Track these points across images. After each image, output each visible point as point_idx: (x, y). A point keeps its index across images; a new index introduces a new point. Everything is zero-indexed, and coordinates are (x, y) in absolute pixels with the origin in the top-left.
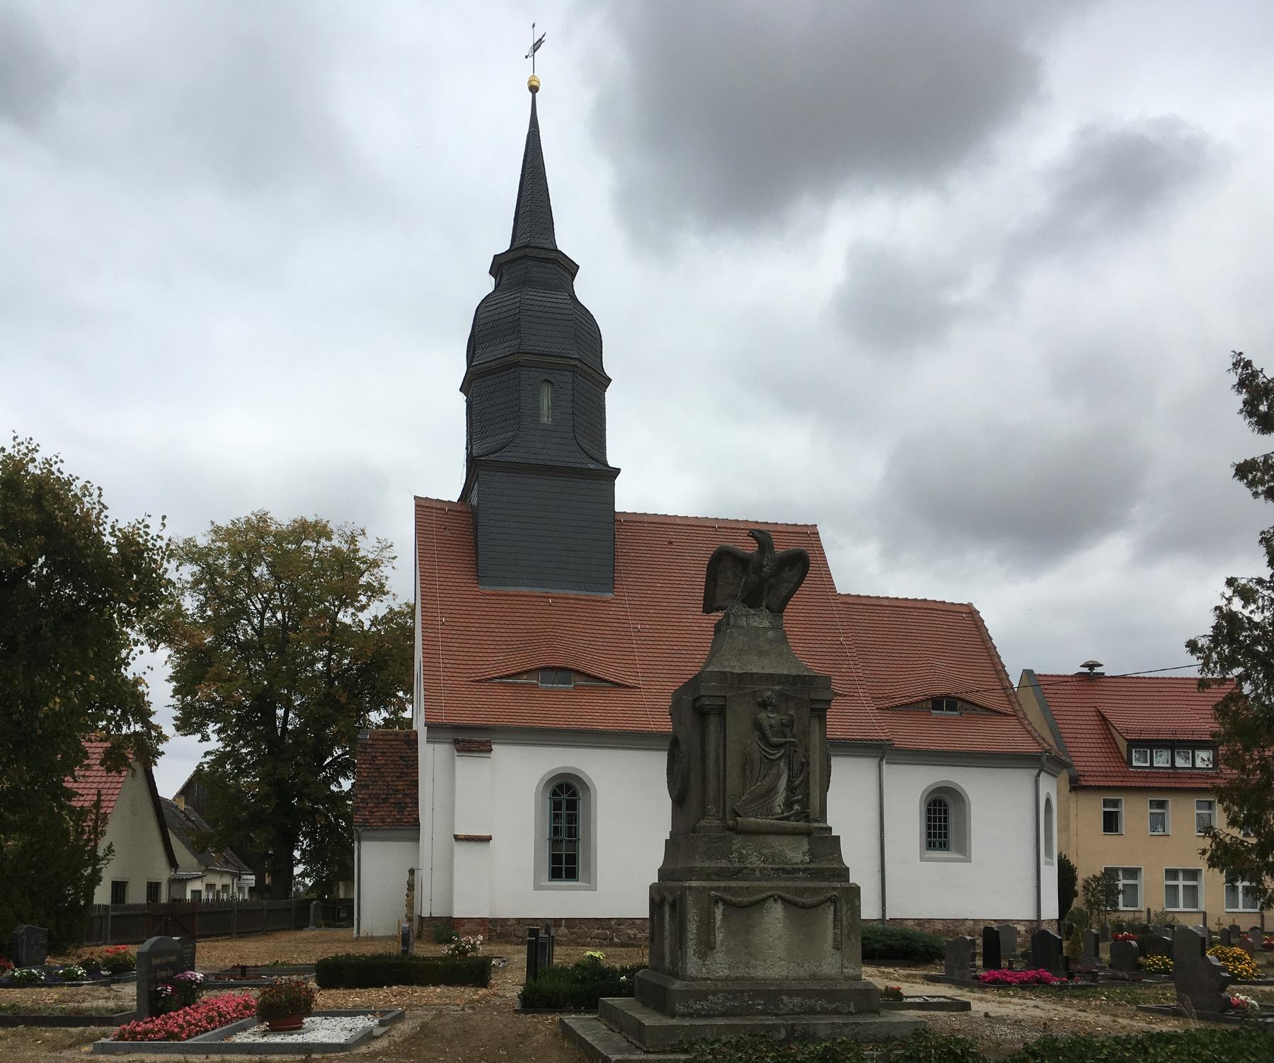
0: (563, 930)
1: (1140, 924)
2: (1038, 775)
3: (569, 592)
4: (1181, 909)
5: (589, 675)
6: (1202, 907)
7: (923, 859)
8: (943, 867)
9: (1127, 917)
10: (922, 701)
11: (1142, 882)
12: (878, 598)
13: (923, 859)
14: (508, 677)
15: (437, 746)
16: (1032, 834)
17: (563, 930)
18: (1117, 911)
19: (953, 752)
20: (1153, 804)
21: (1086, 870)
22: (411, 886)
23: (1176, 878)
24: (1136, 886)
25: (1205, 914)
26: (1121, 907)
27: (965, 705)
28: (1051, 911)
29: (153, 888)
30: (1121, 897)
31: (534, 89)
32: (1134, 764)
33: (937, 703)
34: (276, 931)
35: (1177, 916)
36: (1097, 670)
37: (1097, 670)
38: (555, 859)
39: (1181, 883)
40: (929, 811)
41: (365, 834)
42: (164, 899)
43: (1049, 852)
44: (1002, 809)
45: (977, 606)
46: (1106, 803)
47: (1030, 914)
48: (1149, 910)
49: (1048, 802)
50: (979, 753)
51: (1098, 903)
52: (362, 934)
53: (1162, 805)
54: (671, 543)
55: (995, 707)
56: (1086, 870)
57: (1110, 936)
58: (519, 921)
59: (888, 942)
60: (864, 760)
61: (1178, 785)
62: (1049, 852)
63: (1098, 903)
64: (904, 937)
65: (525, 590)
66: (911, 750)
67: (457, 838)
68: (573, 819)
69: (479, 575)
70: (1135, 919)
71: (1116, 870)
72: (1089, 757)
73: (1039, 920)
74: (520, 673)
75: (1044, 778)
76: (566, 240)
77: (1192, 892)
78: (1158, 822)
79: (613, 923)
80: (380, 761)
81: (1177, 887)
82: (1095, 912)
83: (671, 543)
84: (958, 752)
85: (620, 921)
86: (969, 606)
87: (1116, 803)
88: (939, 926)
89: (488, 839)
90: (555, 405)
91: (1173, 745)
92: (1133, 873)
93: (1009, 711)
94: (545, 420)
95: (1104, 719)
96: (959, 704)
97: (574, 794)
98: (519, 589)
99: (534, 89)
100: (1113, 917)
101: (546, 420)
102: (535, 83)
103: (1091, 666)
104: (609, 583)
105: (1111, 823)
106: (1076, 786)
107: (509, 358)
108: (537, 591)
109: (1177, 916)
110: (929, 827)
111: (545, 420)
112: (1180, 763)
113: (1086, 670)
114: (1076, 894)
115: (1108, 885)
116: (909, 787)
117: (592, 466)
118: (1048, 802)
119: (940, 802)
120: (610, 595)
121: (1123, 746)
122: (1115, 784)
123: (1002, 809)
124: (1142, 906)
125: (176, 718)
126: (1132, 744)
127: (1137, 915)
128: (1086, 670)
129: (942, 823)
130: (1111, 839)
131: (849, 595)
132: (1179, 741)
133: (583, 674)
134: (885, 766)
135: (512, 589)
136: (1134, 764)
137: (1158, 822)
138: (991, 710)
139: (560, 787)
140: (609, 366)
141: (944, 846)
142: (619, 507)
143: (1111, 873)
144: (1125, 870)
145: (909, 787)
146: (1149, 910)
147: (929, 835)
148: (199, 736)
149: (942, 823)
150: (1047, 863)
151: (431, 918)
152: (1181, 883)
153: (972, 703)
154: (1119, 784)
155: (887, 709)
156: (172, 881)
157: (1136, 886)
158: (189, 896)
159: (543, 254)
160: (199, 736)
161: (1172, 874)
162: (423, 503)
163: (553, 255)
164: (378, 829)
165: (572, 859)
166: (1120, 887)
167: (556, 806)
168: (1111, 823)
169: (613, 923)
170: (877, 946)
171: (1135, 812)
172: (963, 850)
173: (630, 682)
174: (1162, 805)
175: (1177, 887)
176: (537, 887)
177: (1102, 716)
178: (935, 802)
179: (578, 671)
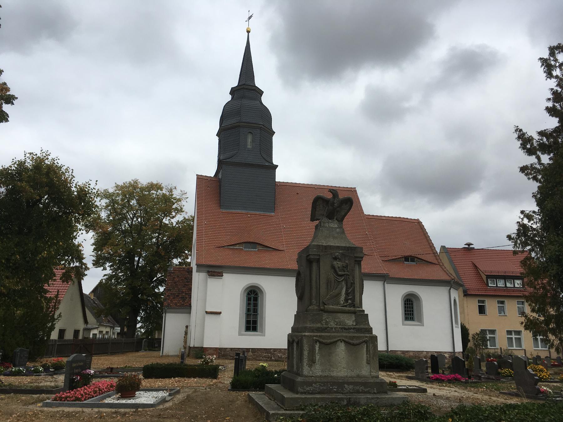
0: (250, 353)
1: (498, 354)
2: (450, 289)
4: (515, 348)
5: (264, 245)
6: (524, 347)
8: (411, 328)
9: (492, 351)
17: (250, 353)
19: (414, 279)
21: (473, 330)
22: (186, 333)
23: (511, 334)
24: (494, 338)
25: (525, 350)
26: (489, 347)
28: (459, 348)
29: (76, 332)
30: (488, 342)
31: (248, 32)
33: (407, 259)
35: (513, 351)
36: (471, 246)
37: (471, 246)
38: (248, 322)
40: (405, 304)
41: (168, 310)
42: (80, 337)
45: (421, 220)
47: (450, 350)
48: (501, 348)
49: (455, 300)
51: (479, 345)
52: (164, 354)
55: (430, 261)
56: (473, 330)
58: (231, 349)
59: (390, 361)
63: (479, 345)
67: (207, 312)
71: (485, 330)
72: (471, 282)
73: (454, 352)
74: (235, 244)
75: (452, 290)
76: (259, 83)
77: (519, 340)
78: (501, 310)
82: (478, 349)
84: (416, 279)
85: (275, 350)
87: (483, 302)
88: (411, 354)
90: (253, 141)
91: (505, 278)
92: (493, 332)
93: (436, 262)
94: (249, 147)
96: (416, 259)
97: (257, 294)
99: (248, 32)
100: (486, 351)
101: (249, 146)
103: (469, 245)
105: (482, 310)
106: (466, 294)
108: (244, 212)
109: (513, 351)
110: (405, 311)
111: (249, 147)
113: (467, 246)
115: (483, 337)
116: (396, 293)
118: (455, 300)
120: (273, 214)
121: (484, 277)
123: (436, 303)
124: (498, 346)
126: (488, 277)
127: (496, 350)
128: (467, 246)
129: (411, 309)
130: (482, 317)
134: (386, 285)
137: (501, 310)
139: (251, 291)
141: (412, 319)
143: (483, 332)
144: (489, 330)
146: (501, 348)
147: (406, 314)
148: (102, 268)
149: (411, 309)
150: (456, 327)
151: (194, 347)
152: (514, 336)
157: (494, 338)
158: (91, 336)
159: (250, 87)
160: (102, 268)
161: (509, 332)
163: (254, 88)
165: (255, 322)
166: (488, 338)
167: (249, 299)
168: (482, 310)
169: (272, 350)
170: (385, 363)
171: (491, 305)
172: (420, 321)
173: (281, 248)
174: (502, 302)
175: (512, 338)
176: (240, 334)
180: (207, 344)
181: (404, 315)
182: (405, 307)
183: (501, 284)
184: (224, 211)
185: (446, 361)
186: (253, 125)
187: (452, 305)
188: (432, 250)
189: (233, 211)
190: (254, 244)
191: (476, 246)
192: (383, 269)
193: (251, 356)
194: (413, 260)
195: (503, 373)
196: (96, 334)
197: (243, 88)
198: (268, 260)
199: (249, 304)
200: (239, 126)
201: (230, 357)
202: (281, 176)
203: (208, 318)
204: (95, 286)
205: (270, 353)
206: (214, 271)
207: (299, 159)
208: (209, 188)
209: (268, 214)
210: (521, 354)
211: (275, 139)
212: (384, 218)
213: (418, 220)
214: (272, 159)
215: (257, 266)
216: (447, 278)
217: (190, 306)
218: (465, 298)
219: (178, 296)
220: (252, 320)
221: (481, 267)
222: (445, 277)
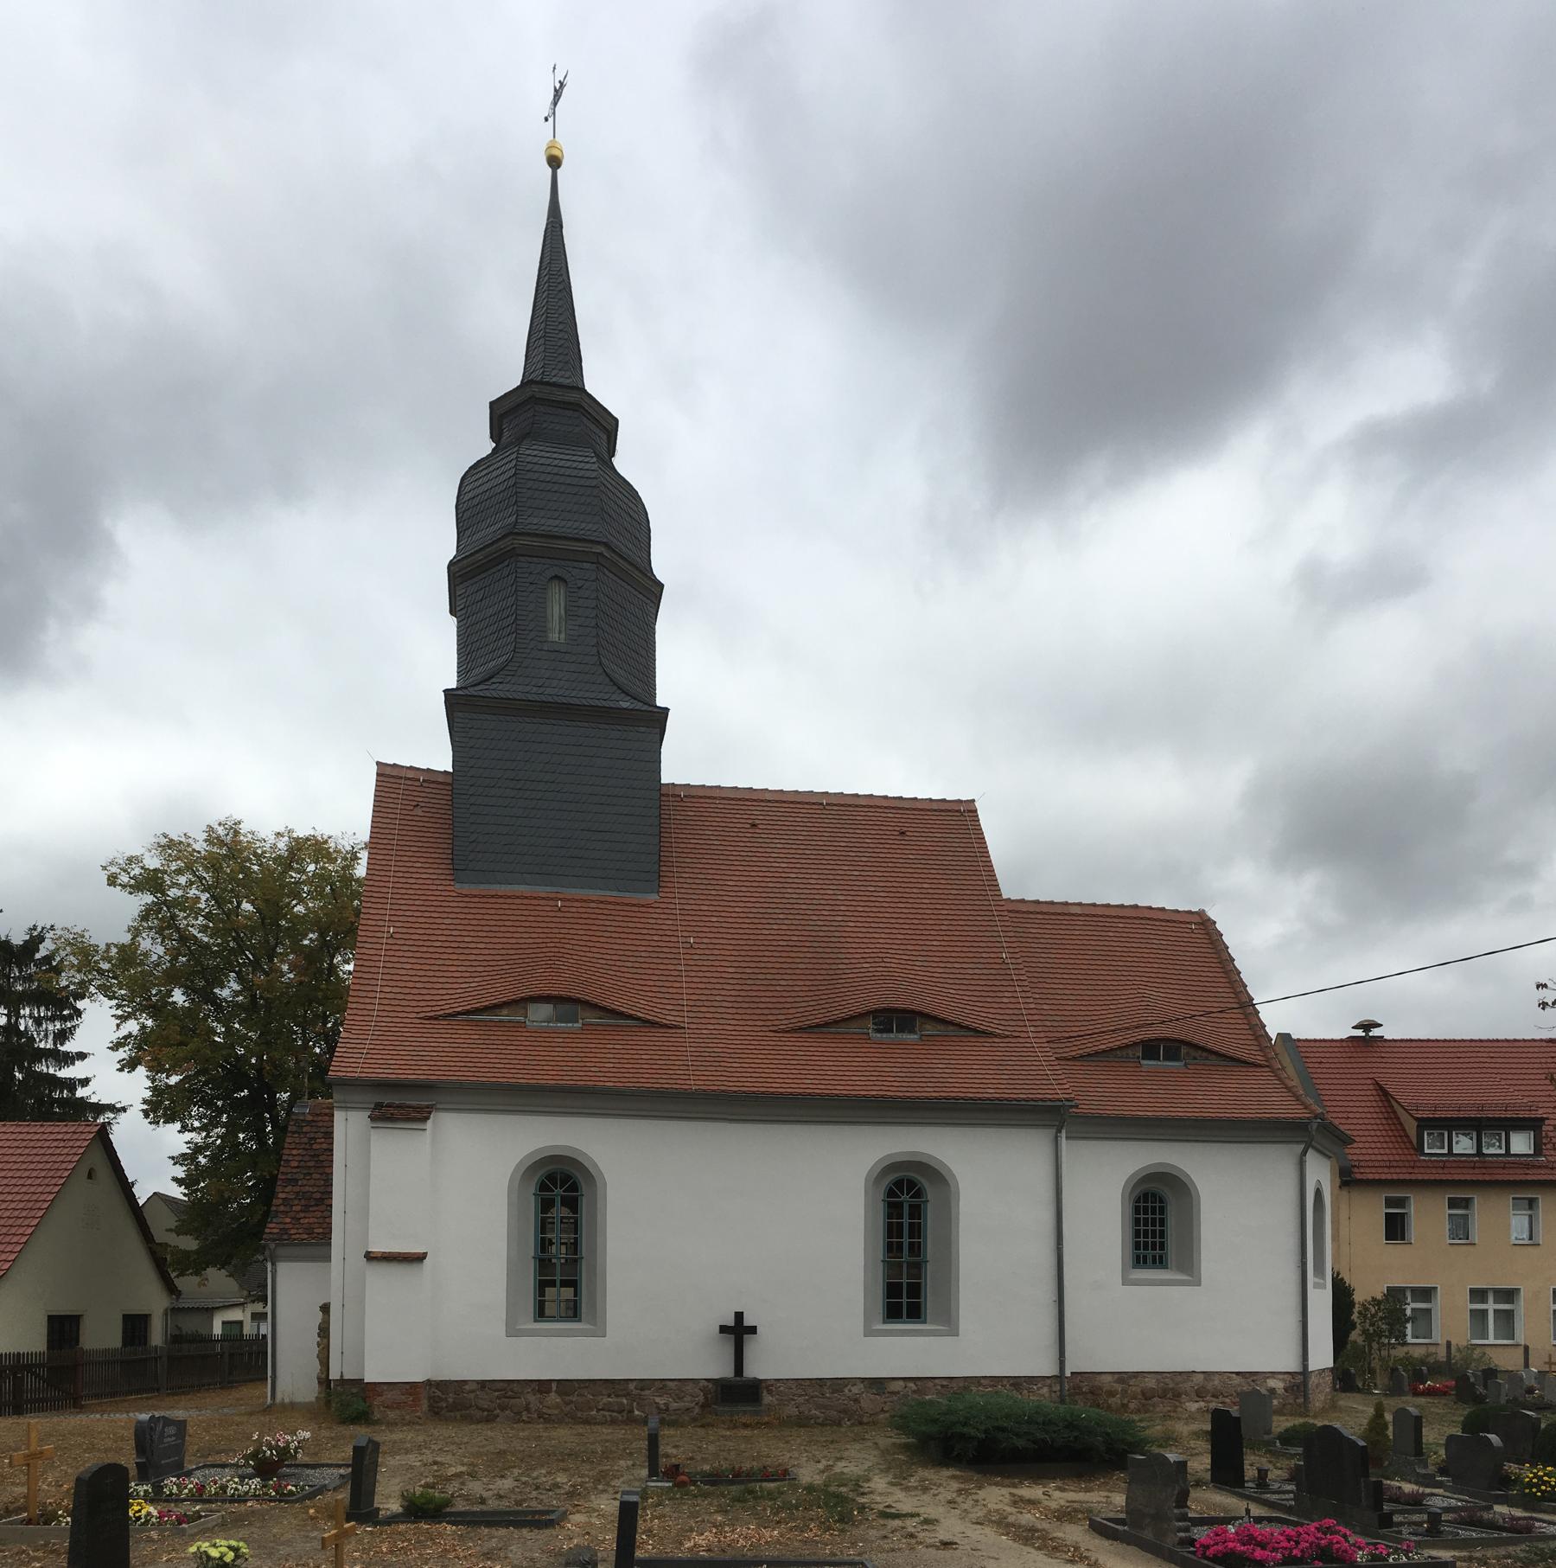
0: (553, 1398)
1: (1437, 1362)
2: (1304, 1153)
3: (591, 892)
4: (1491, 1341)
5: (604, 1009)
6: (1520, 1337)
7: (1126, 1282)
8: (1158, 1295)
9: (1418, 1353)
10: (1127, 1046)
11: (1438, 1305)
12: (1066, 904)
13: (1126, 1282)
14: (467, 1013)
15: (350, 1114)
16: (1292, 1243)
17: (553, 1398)
18: (1405, 1344)
19: (1173, 1119)
20: (1453, 1203)
21: (1366, 1290)
22: (324, 1331)
23: (1484, 1301)
24: (1429, 1311)
25: (1526, 1348)
26: (1409, 1339)
27: (1193, 1053)
28: (1322, 1356)
29: (135, 1326)
30: (1409, 1326)
31: (554, 162)
32: (1427, 1151)
33: (1150, 1049)
34: (251, 1381)
35: (1488, 1351)
36: (1375, 1032)
37: (1375, 1032)
38: (892, 1290)
39: (1491, 1306)
40: (1137, 1210)
41: (281, 1251)
42: (157, 1337)
43: (1319, 1270)
44: (1249, 1207)
45: (1212, 914)
46: (1390, 1202)
47: (1290, 1363)
48: (1449, 1344)
49: (1318, 1194)
50: (1213, 1120)
51: (1380, 1334)
52: (278, 1399)
53: (1466, 1204)
54: (754, 825)
55: (1238, 1055)
56: (1366, 1290)
57: (1407, 1388)
58: (483, 1384)
59: (1040, 1435)
60: (1033, 1132)
61: (1487, 1178)
62: (1319, 1270)
63: (1380, 1334)
64: (1070, 1425)
66: (1109, 1117)
67: (370, 1257)
70: (1429, 1355)
71: (1402, 1290)
72: (1370, 1148)
73: (1305, 1372)
75: (1311, 1157)
76: (602, 379)
77: (1506, 1318)
78: (1461, 1230)
79: (632, 1386)
81: (1485, 1312)
82: (1375, 1345)
83: (754, 825)
84: (1181, 1119)
85: (644, 1384)
87: (1401, 1202)
88: (1151, 1383)
89: (419, 1258)
90: (569, 614)
91: (1477, 1125)
92: (1426, 1294)
93: (1260, 1059)
94: (554, 636)
95: (1383, 1093)
96: (1184, 1050)
97: (575, 1187)
98: (516, 887)
99: (554, 162)
100: (1400, 1352)
101: (556, 635)
102: (555, 152)
103: (1367, 1026)
104: (655, 878)
105: (1395, 1228)
106: (1348, 1180)
108: (542, 891)
109: (1488, 1351)
110: (1137, 1234)
111: (554, 636)
112: (1493, 1150)
113: (1360, 1033)
114: (1353, 1326)
115: (1395, 1309)
116: (1102, 1178)
117: (624, 705)
118: (1318, 1194)
119: (1154, 1195)
120: (655, 897)
121: (1411, 1127)
122: (1402, 1177)
123: (1249, 1207)
124: (1438, 1337)
125: (145, 1102)
126: (1424, 1124)
127: (1432, 1349)
128: (1360, 1033)
129: (1157, 1228)
130: (1395, 1251)
131: (1023, 901)
132: (1489, 1119)
133: (595, 1006)
134: (1064, 1142)
136: (1427, 1151)
137: (1461, 1230)
138: (1232, 1059)
139: (551, 1177)
140: (661, 565)
141: (1160, 1262)
143: (1395, 1294)
144: (1413, 1290)
145: (1102, 1178)
146: (1449, 1344)
147: (1137, 1246)
148: (178, 1125)
149: (1157, 1228)
150: (1316, 1286)
152: (1491, 1306)
153: (1203, 1049)
154: (1407, 1177)
155: (1074, 1058)
156: (174, 1311)
157: (1429, 1311)
158: (217, 1330)
159: (559, 395)
160: (178, 1125)
161: (1478, 1295)
162: (388, 771)
163: (573, 397)
164: (301, 1243)
165: (916, 1290)
166: (1408, 1312)
167: (546, 1205)
168: (1395, 1228)
169: (632, 1386)
170: (1020, 1443)
171: (1428, 1216)
172: (1189, 1268)
173: (670, 1019)
174: (1466, 1204)
175: (1485, 1312)
176: (512, 1331)
177: (1381, 1088)
178: (1146, 1195)
179: (587, 1003)
180: (373, 1374)
181: (1130, 1245)
182: (1137, 1222)
183: (1464, 1145)
184: (466, 889)
185: (1275, 1402)
187: (1309, 1215)
188: (1246, 1016)
191: (1387, 1032)
192: (1055, 1084)
193: (557, 1406)
194: (1172, 1055)
195: (1530, 1485)
196: (241, 1323)
198: (610, 1060)
199: (544, 1226)
201: (478, 1414)
202: (684, 761)
205: (628, 1395)
206: (402, 1104)
207: (754, 695)
208: (418, 811)
209: (629, 897)
210: (1507, 1361)
212: (1078, 910)
213: (1201, 914)
214: (654, 696)
216: (1298, 1112)
217: (325, 1237)
218: (1345, 1193)
220: (905, 1281)
221: (1404, 1094)
222: (1287, 1110)
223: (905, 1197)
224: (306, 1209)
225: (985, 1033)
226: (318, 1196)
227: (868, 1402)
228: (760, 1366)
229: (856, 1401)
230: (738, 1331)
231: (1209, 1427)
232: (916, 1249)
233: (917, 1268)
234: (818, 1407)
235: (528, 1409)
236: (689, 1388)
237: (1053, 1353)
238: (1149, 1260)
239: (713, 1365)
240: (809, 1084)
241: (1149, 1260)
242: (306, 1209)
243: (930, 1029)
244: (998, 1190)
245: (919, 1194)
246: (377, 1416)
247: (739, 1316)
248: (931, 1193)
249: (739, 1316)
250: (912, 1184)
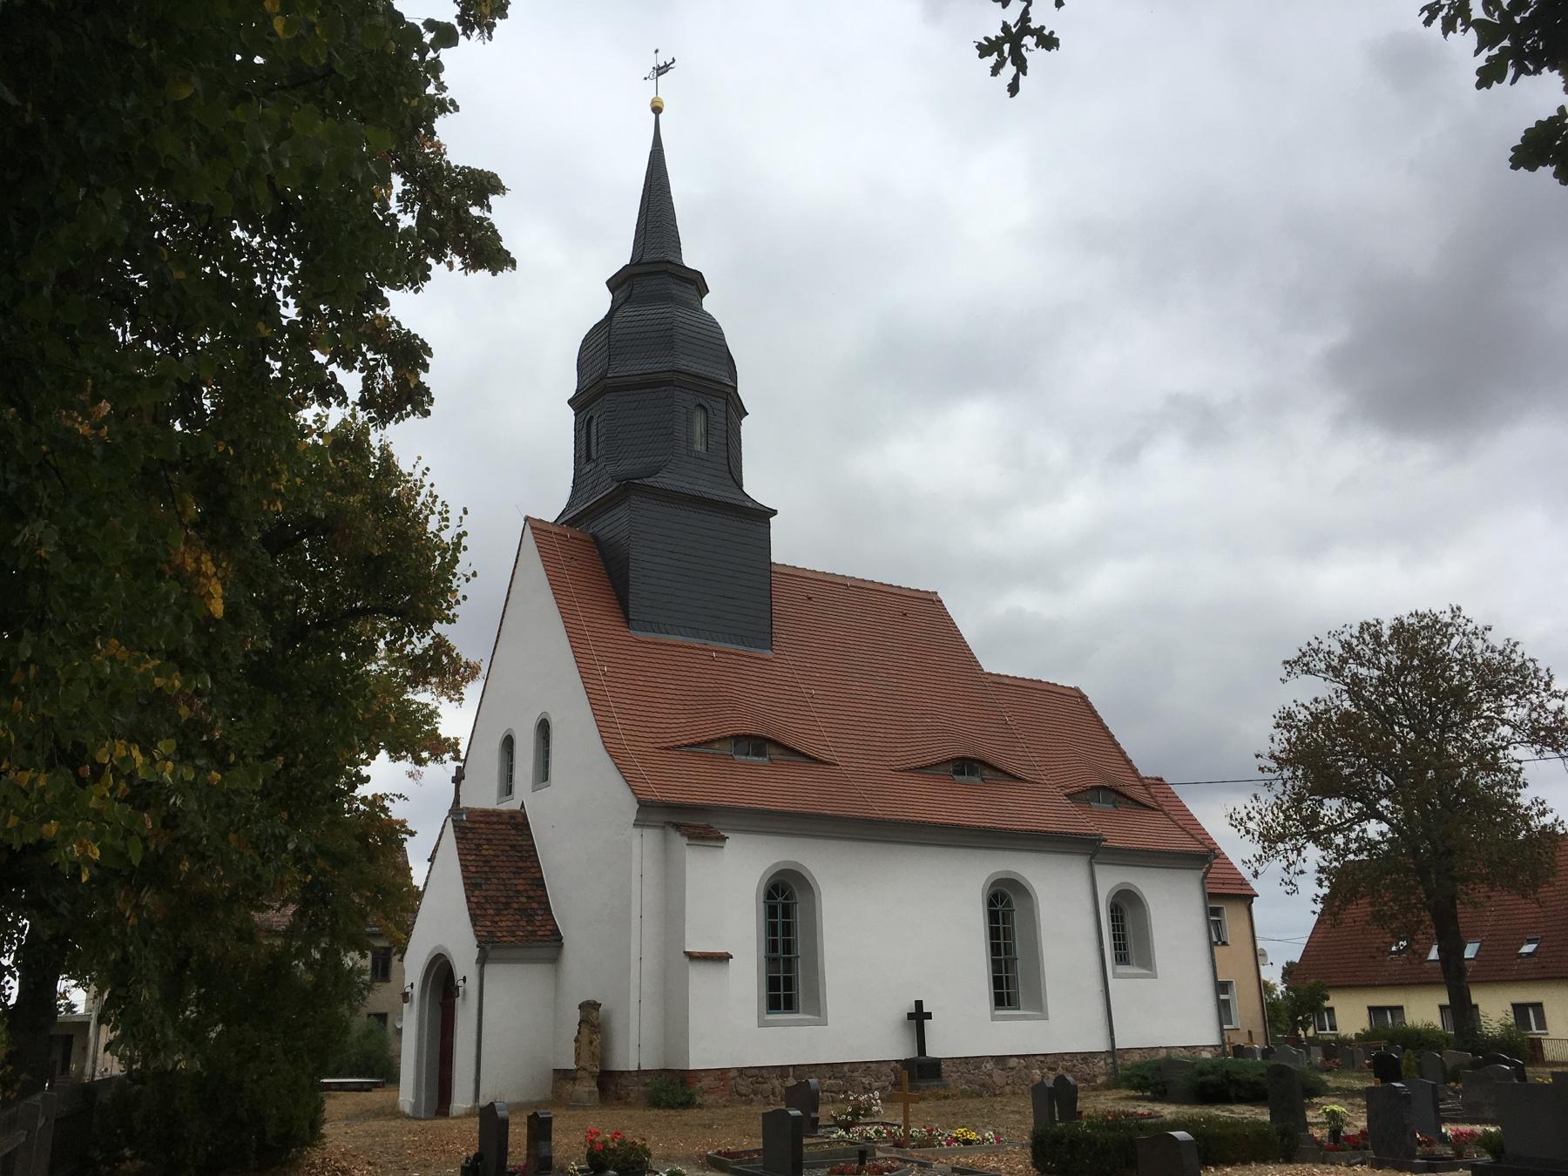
14: (693, 745)
31: (657, 110)
38: (773, 984)
52: (901, 1105)
58: (741, 1071)
60: (1068, 858)
65: (679, 639)
68: (788, 929)
69: (628, 621)
74: (713, 741)
80: (487, 851)
86: (1077, 690)
89: (723, 958)
93: (1153, 804)
99: (657, 110)
101: (699, 447)
107: (661, 376)
108: (696, 642)
120: (769, 654)
134: (1097, 868)
135: (680, 638)
142: (778, 556)
151: (640, 1072)
162: (538, 525)
165: (789, 983)
167: (771, 912)
169: (846, 1068)
173: (826, 758)
176: (762, 1024)
180: (699, 1058)
184: (641, 635)
186: (705, 383)
189: (664, 638)
190: (757, 744)
197: (666, 271)
200: (669, 383)
203: (699, 977)
204: (459, 869)
211: (749, 429)
215: (878, 812)
219: (507, 905)
220: (781, 975)
223: (780, 899)
224: (498, 912)
225: (1014, 777)
226: (503, 900)
227: (999, 1077)
228: (933, 1051)
229: (990, 1076)
230: (919, 1016)
231: (758, 1144)
232: (788, 947)
233: (789, 964)
234: (968, 1082)
235: (773, 1093)
236: (886, 1069)
237: (1104, 1032)
238: (774, 955)
239: (892, 1047)
240: (942, 817)
241: (774, 955)
242: (498, 912)
243: (987, 773)
244: (1064, 902)
245: (1009, 903)
246: (699, 1100)
247: (919, 1004)
248: (1016, 904)
249: (919, 1004)
250: (1004, 895)
